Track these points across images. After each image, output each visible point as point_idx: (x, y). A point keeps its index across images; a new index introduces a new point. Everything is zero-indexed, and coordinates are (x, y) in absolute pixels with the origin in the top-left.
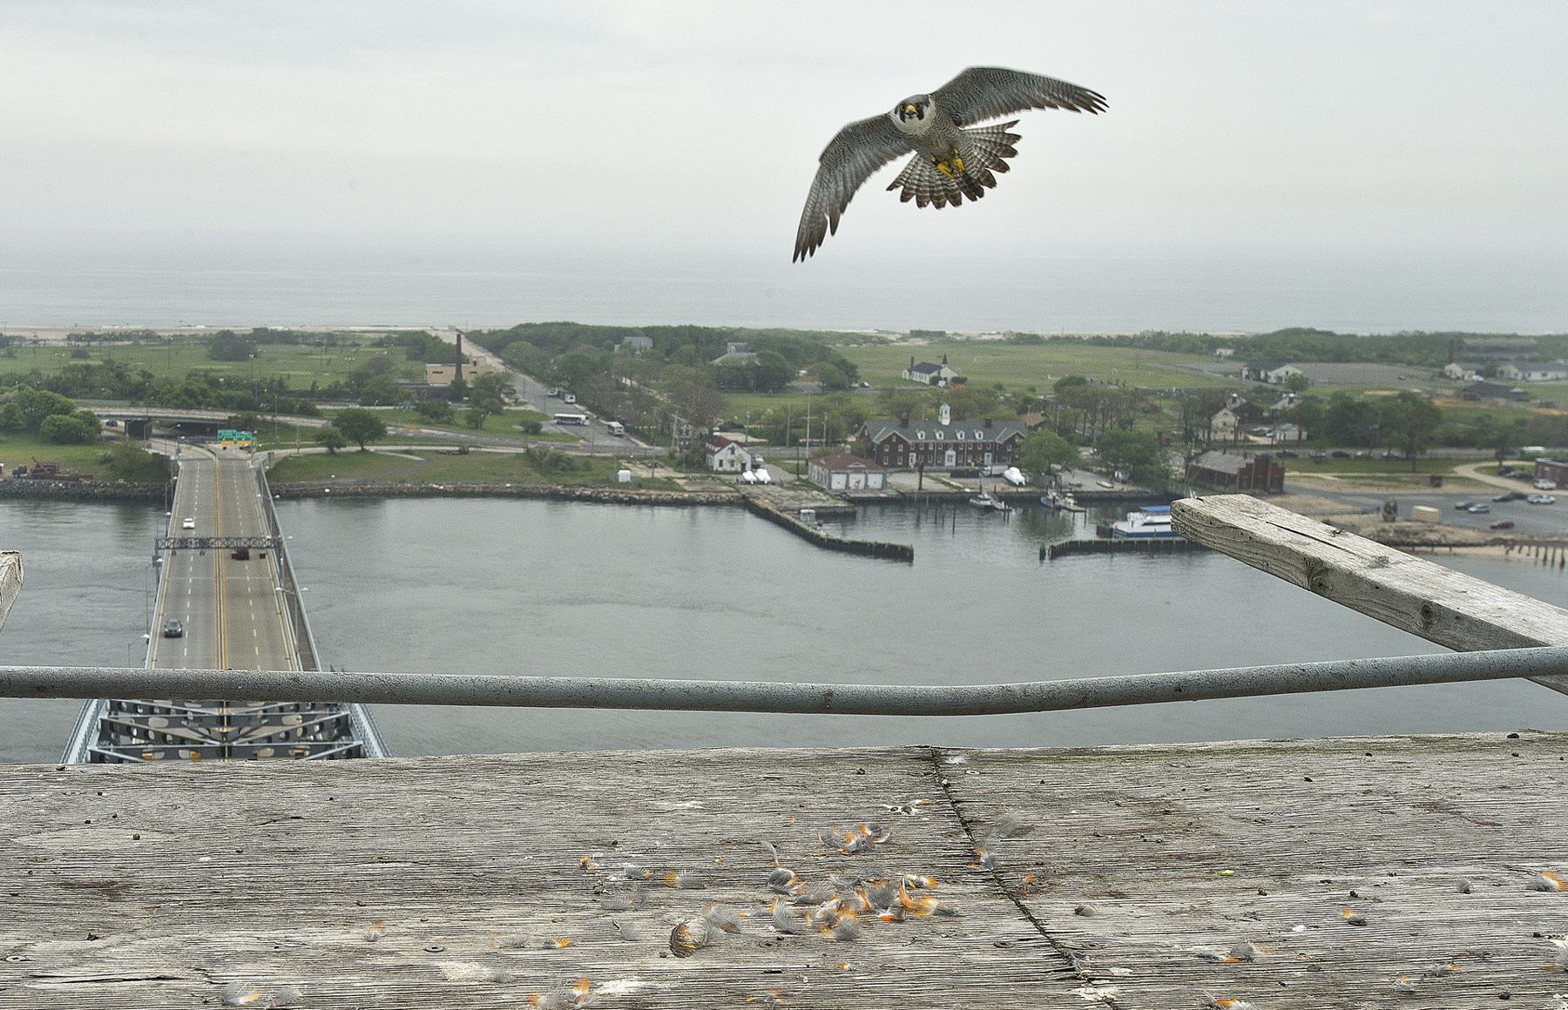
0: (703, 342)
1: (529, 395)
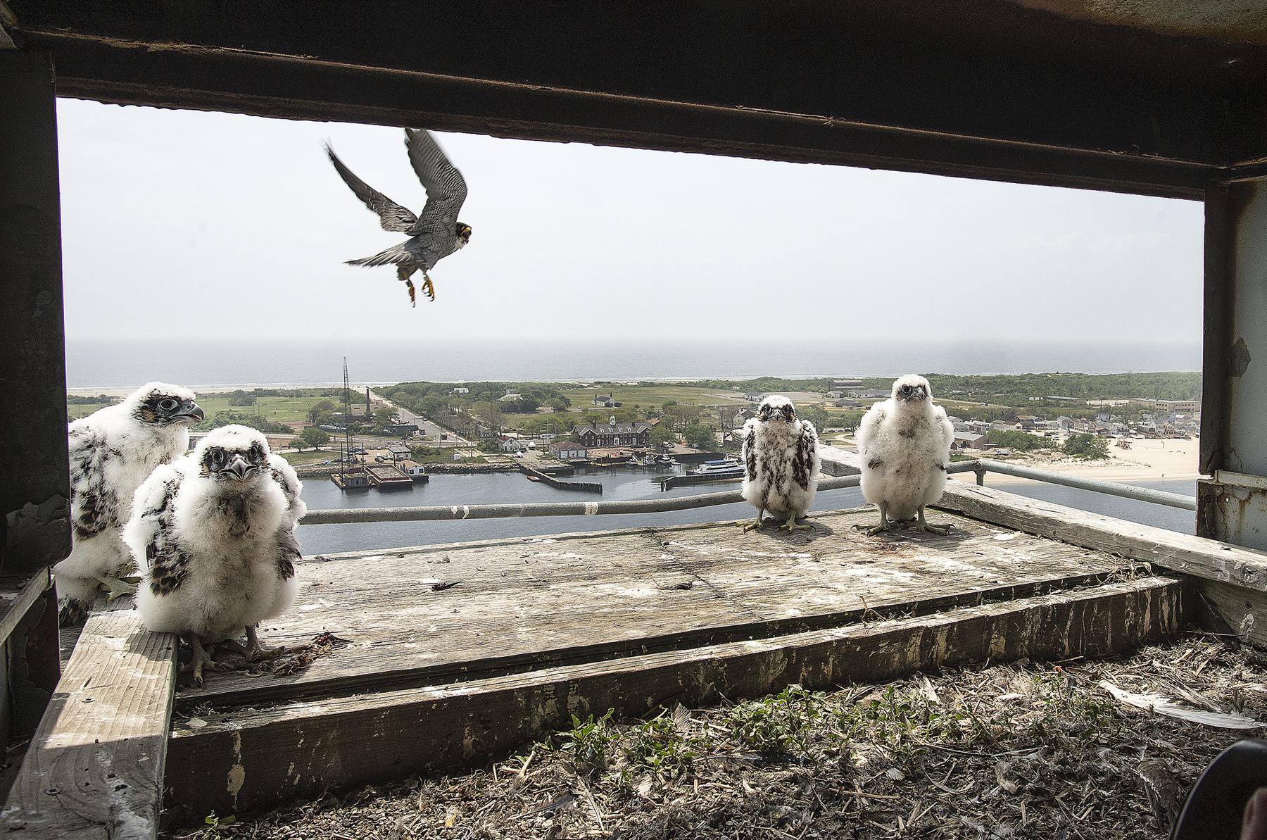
0: (495, 390)
1: (406, 416)
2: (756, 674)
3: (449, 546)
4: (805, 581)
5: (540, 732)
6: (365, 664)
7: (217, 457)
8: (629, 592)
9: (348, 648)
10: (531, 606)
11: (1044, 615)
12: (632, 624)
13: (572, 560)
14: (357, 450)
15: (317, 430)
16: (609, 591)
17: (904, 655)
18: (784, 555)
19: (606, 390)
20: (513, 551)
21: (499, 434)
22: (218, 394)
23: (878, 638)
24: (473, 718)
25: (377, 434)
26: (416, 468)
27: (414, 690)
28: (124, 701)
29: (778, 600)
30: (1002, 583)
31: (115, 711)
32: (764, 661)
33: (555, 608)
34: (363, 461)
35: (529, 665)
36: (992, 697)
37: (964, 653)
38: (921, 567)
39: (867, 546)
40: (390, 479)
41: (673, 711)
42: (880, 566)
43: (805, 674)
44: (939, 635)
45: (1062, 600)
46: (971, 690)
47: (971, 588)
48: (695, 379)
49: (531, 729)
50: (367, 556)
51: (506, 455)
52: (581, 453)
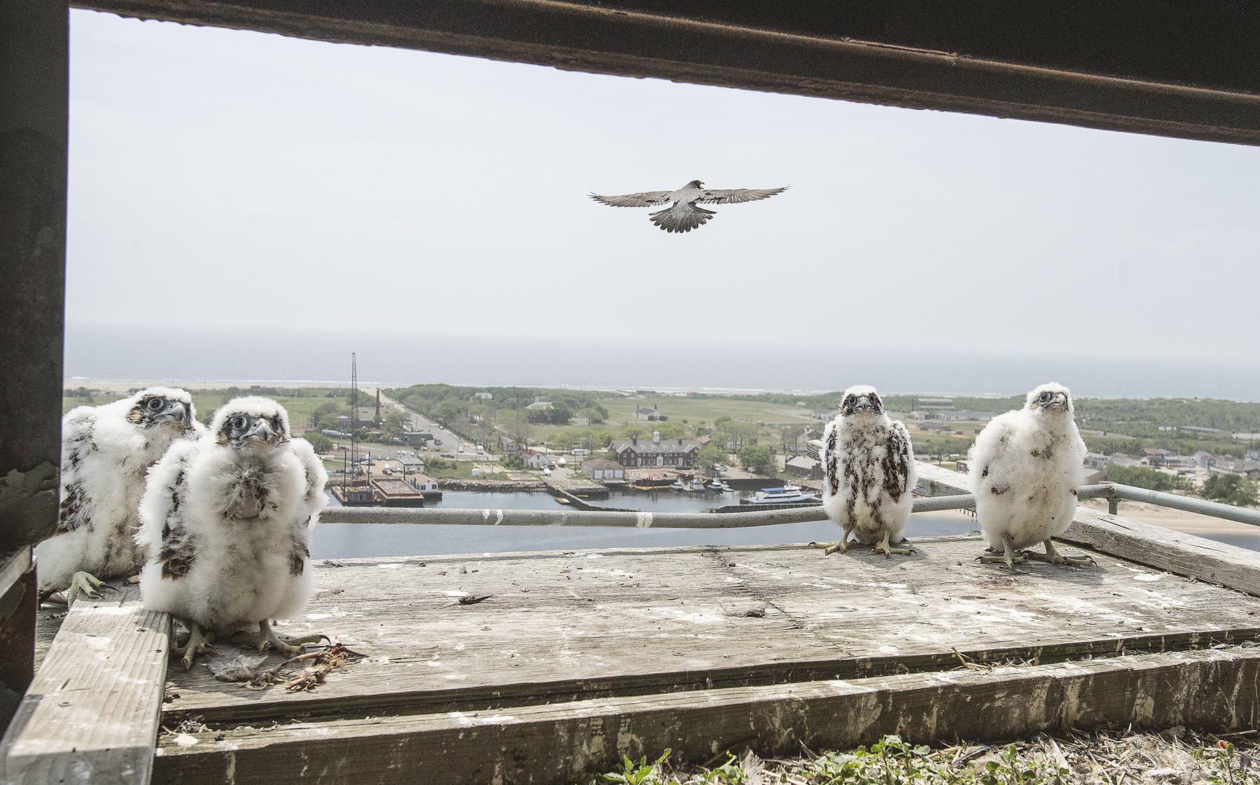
1: (419, 424)
2: (844, 721)
3: (477, 556)
4: (900, 615)
5: (584, 775)
6: (382, 682)
7: (240, 423)
8: (689, 618)
9: (362, 663)
10: (574, 626)
11: (1205, 674)
12: (695, 653)
13: (621, 578)
14: (362, 460)
15: (319, 435)
16: (665, 615)
17: (1025, 711)
18: (874, 584)
19: (649, 402)
20: (552, 565)
21: (525, 447)
22: (210, 391)
23: (994, 687)
24: (505, 753)
25: (388, 443)
26: (428, 483)
27: (437, 715)
28: (107, 706)
29: (870, 635)
30: (1148, 630)
31: (95, 717)
32: (853, 706)
33: (603, 631)
34: (369, 473)
35: (573, 693)
36: (1140, 771)
37: (1101, 714)
38: (1044, 606)
39: (975, 579)
40: (398, 495)
41: (743, 759)
42: (993, 603)
43: (904, 726)
44: (1070, 688)
45: (1227, 657)
46: (1111, 760)
47: (1109, 634)
48: (755, 391)
49: (572, 771)
50: (384, 563)
51: (532, 472)
52: (619, 473)
